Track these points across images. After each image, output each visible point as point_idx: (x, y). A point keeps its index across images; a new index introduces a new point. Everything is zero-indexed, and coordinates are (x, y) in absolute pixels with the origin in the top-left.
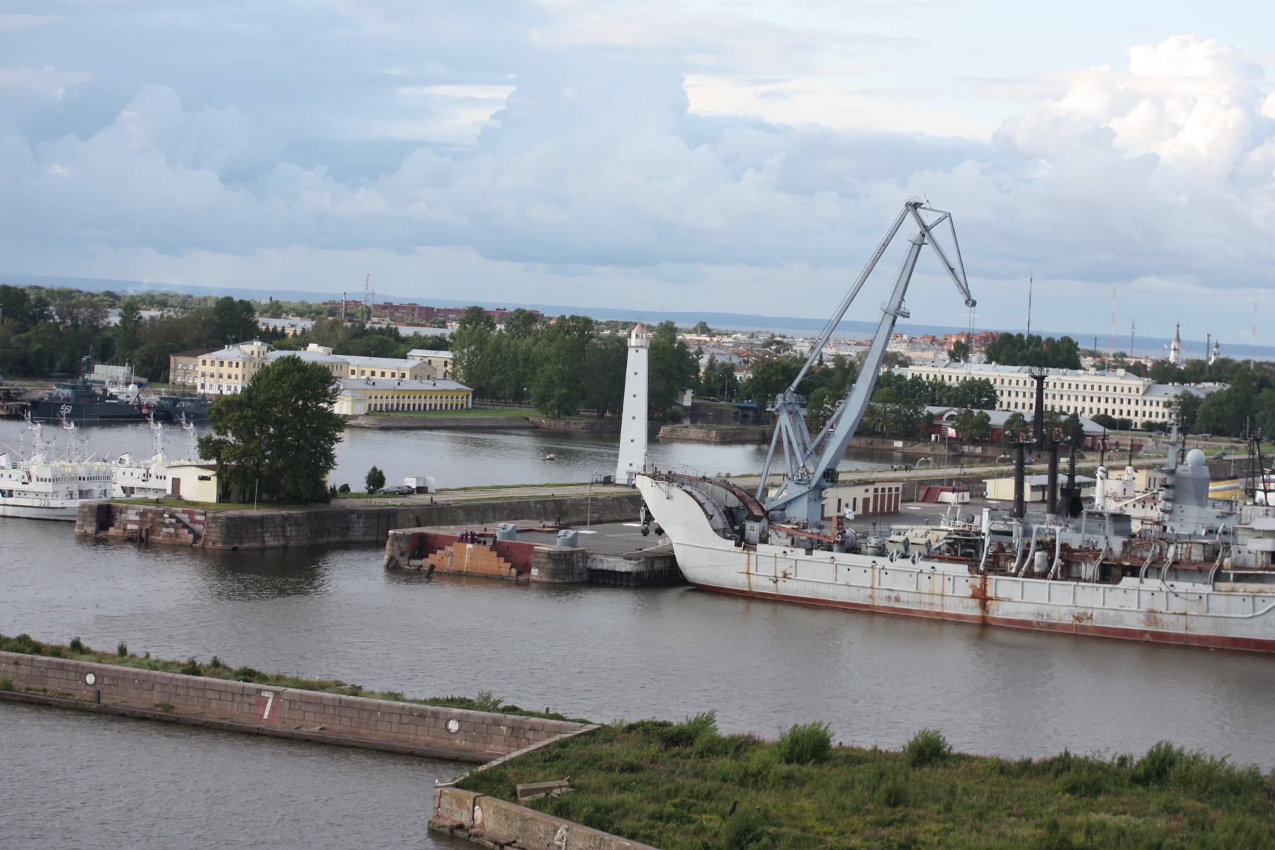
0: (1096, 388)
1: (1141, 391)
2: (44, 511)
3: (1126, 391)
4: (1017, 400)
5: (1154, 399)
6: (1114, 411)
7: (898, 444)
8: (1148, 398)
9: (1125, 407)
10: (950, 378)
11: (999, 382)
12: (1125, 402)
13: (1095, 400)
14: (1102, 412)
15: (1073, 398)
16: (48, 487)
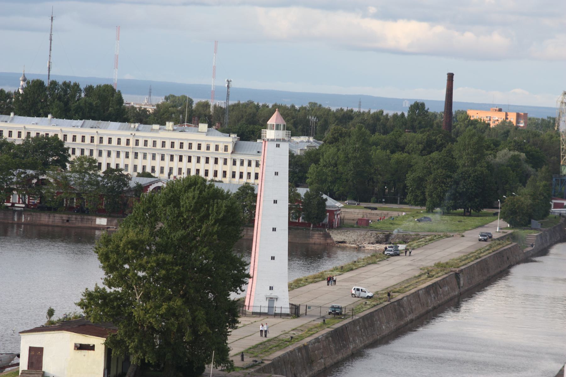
0: (186, 146)
1: (230, 149)
3: (212, 148)
4: (207, 167)
5: (246, 158)
7: (102, 221)
8: (238, 157)
9: (211, 167)
10: (10, 133)
11: (70, 139)
12: (203, 160)
13: (176, 159)
14: (193, 173)
15: (149, 157)
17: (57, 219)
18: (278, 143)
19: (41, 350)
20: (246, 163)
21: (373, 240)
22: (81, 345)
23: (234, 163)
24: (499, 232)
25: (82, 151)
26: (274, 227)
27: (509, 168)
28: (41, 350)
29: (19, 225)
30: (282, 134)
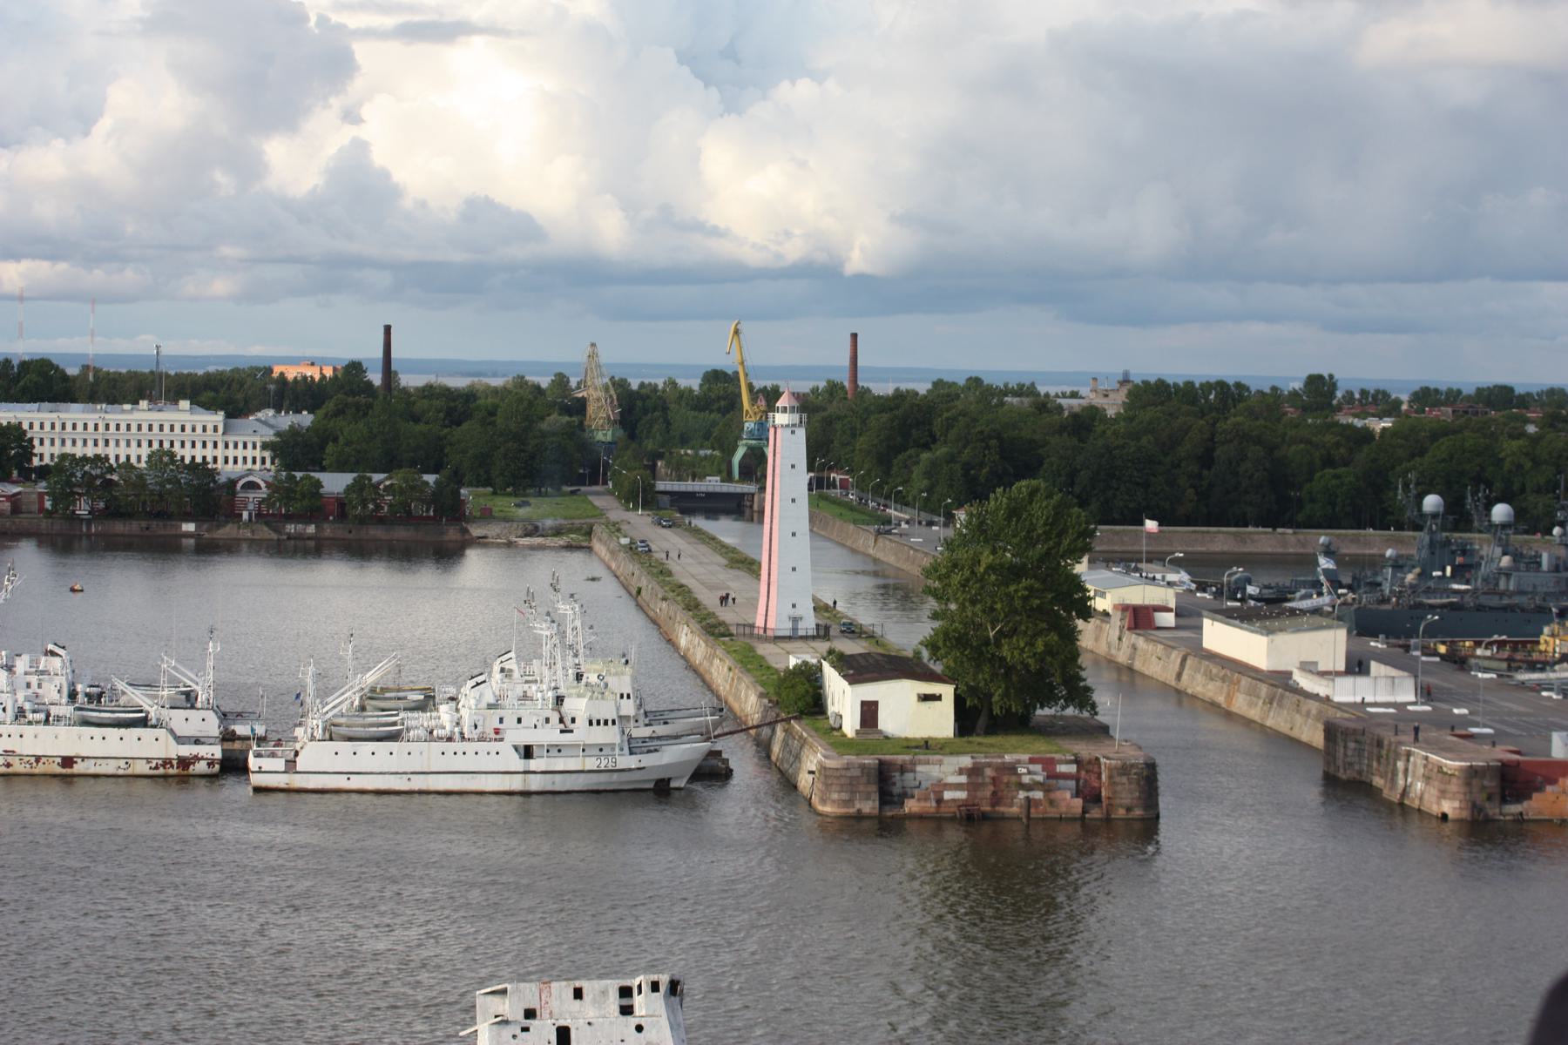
1: (221, 429)
2: (603, 777)
3: (199, 430)
6: (215, 459)
7: (189, 527)
8: (231, 439)
11: (37, 427)
16: (611, 735)
17: (134, 527)
19: (876, 704)
20: (240, 446)
21: (520, 532)
23: (227, 446)
25: (161, 443)
28: (876, 704)
29: (89, 536)
30: (796, 418)
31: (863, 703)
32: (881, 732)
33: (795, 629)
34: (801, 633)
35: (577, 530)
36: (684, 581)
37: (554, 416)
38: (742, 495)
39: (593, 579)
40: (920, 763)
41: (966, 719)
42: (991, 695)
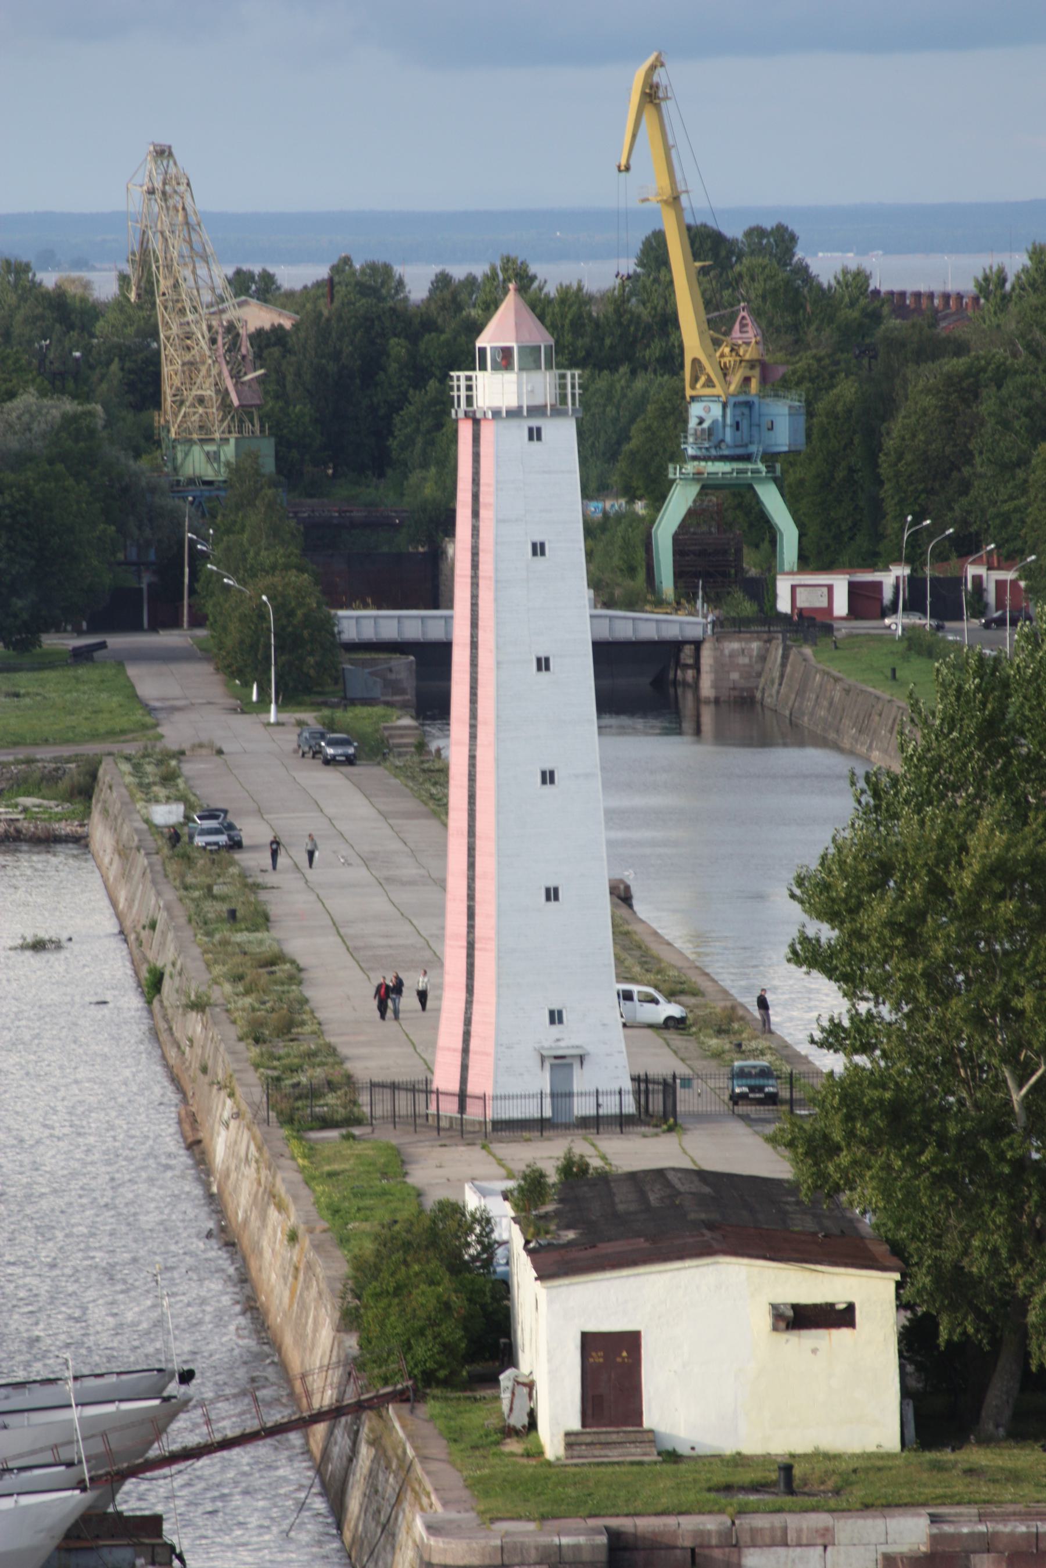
18: (535, 423)
19: (631, 1341)
22: (795, 1307)
24: (278, 724)
26: (547, 767)
27: (60, 467)
28: (631, 1341)
30: (542, 385)
31: (589, 1341)
32: (651, 1437)
33: (561, 1096)
34: (583, 1107)
35: (45, 782)
36: (297, 946)
37: (28, 398)
38: (676, 646)
39: (38, 946)
40: (757, 1540)
41: (943, 1392)
42: (1022, 1306)
